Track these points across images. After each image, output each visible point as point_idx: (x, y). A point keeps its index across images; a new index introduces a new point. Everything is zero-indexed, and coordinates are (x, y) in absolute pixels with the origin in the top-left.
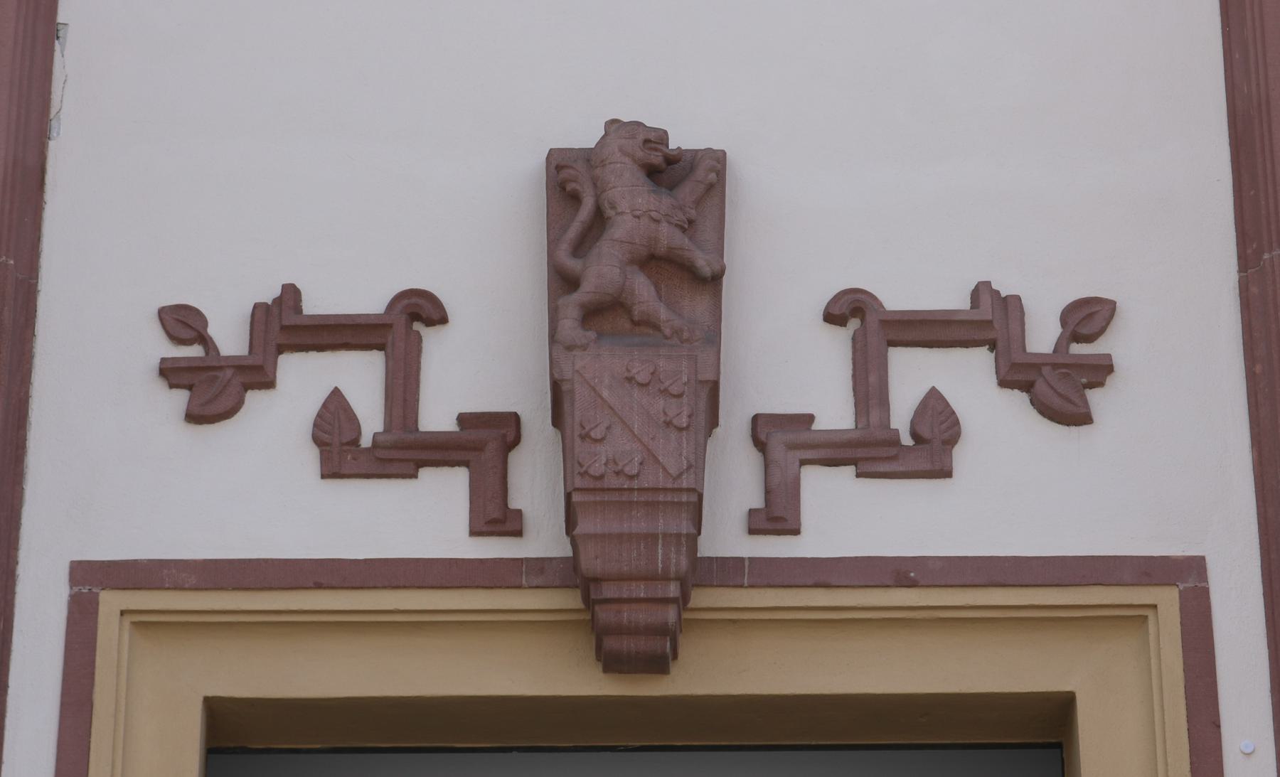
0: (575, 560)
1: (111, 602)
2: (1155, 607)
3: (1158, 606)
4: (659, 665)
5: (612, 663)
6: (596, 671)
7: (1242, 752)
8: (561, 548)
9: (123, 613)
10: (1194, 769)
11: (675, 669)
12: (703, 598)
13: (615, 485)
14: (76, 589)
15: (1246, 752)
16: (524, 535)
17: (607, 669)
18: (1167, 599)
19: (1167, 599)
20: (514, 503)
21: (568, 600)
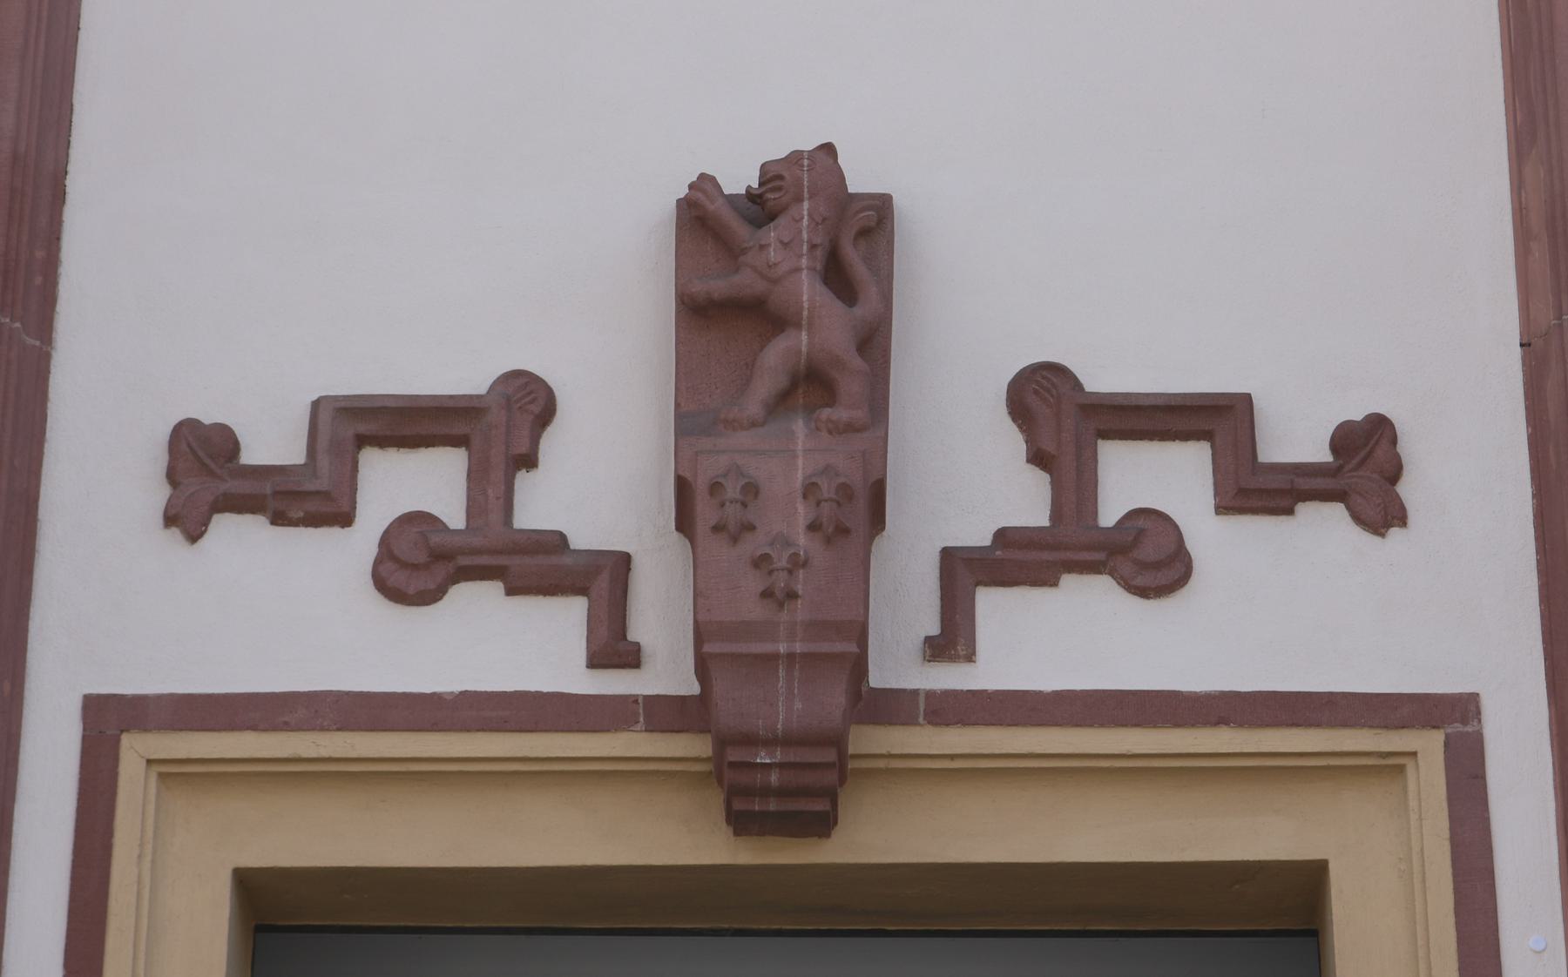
0: (704, 699)
1: (135, 750)
2: (1414, 754)
3: (1419, 755)
4: (822, 825)
5: (742, 823)
6: (724, 831)
7: (1531, 950)
8: (689, 686)
9: (149, 762)
10: (1463, 969)
11: (837, 834)
12: (870, 740)
13: (689, 610)
14: (921, 720)
15: (1537, 950)
16: (589, 670)
17: (738, 833)
18: (1429, 745)
19: (1429, 745)
20: (634, 634)
21: (691, 746)
